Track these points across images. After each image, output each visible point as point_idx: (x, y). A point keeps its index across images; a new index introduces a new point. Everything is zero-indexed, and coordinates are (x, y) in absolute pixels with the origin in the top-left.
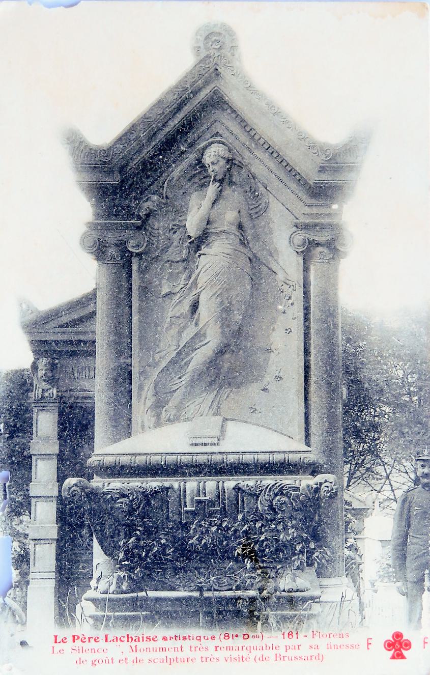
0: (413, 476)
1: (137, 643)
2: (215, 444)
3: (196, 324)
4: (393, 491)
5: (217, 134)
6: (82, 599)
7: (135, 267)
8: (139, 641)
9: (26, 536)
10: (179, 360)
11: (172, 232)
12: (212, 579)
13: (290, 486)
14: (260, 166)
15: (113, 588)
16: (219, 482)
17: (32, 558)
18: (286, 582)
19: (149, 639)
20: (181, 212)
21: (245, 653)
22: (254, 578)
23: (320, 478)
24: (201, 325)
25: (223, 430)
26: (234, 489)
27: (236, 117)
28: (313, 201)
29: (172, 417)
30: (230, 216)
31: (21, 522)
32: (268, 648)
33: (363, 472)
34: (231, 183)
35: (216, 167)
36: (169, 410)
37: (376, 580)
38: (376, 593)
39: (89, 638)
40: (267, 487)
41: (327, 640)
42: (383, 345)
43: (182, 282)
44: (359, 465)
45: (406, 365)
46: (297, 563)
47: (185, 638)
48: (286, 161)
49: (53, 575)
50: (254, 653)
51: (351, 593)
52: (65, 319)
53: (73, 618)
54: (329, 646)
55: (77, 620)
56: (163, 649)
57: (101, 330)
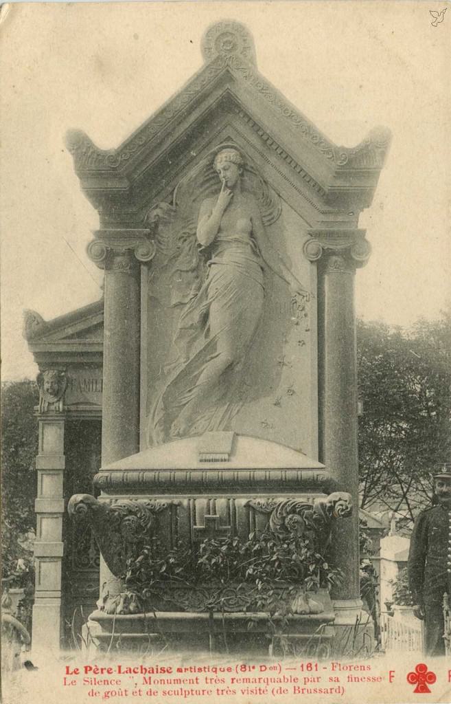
0: (430, 495)
1: (151, 675)
2: (225, 460)
3: (207, 336)
4: (410, 510)
5: (229, 139)
6: (89, 619)
7: (143, 277)
8: (153, 672)
9: (31, 553)
10: (187, 376)
11: (182, 240)
12: (223, 599)
13: (302, 504)
14: (274, 171)
15: (119, 609)
16: (229, 500)
17: (37, 575)
18: (298, 604)
19: (163, 670)
20: (189, 220)
21: (263, 686)
22: (265, 599)
23: (334, 496)
24: (212, 335)
25: (234, 442)
26: (245, 506)
27: (249, 121)
28: (326, 208)
29: (181, 432)
30: (242, 223)
31: (27, 539)
32: (286, 680)
33: (378, 490)
34: (243, 190)
35: (228, 174)
36: (180, 424)
37: (393, 603)
38: (392, 616)
39: (102, 669)
40: (279, 505)
41: (347, 673)
42: (401, 358)
43: (192, 292)
44: (375, 483)
45: (423, 378)
46: (310, 585)
47: (200, 670)
48: (295, 162)
49: (59, 594)
50: (272, 686)
51: (366, 617)
52: (70, 331)
53: (79, 640)
54: (350, 679)
55: (83, 641)
56: (178, 681)
57: (108, 341)
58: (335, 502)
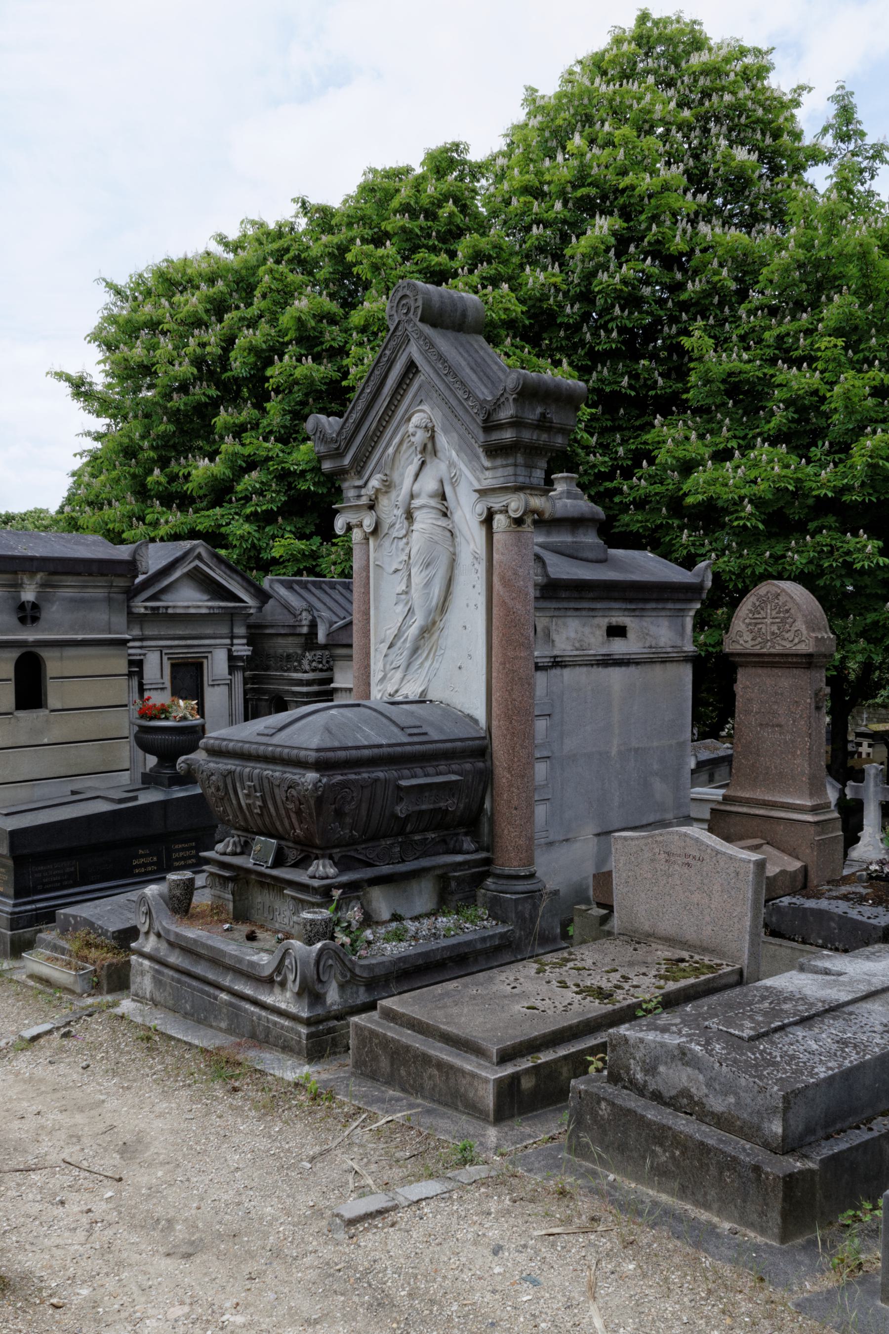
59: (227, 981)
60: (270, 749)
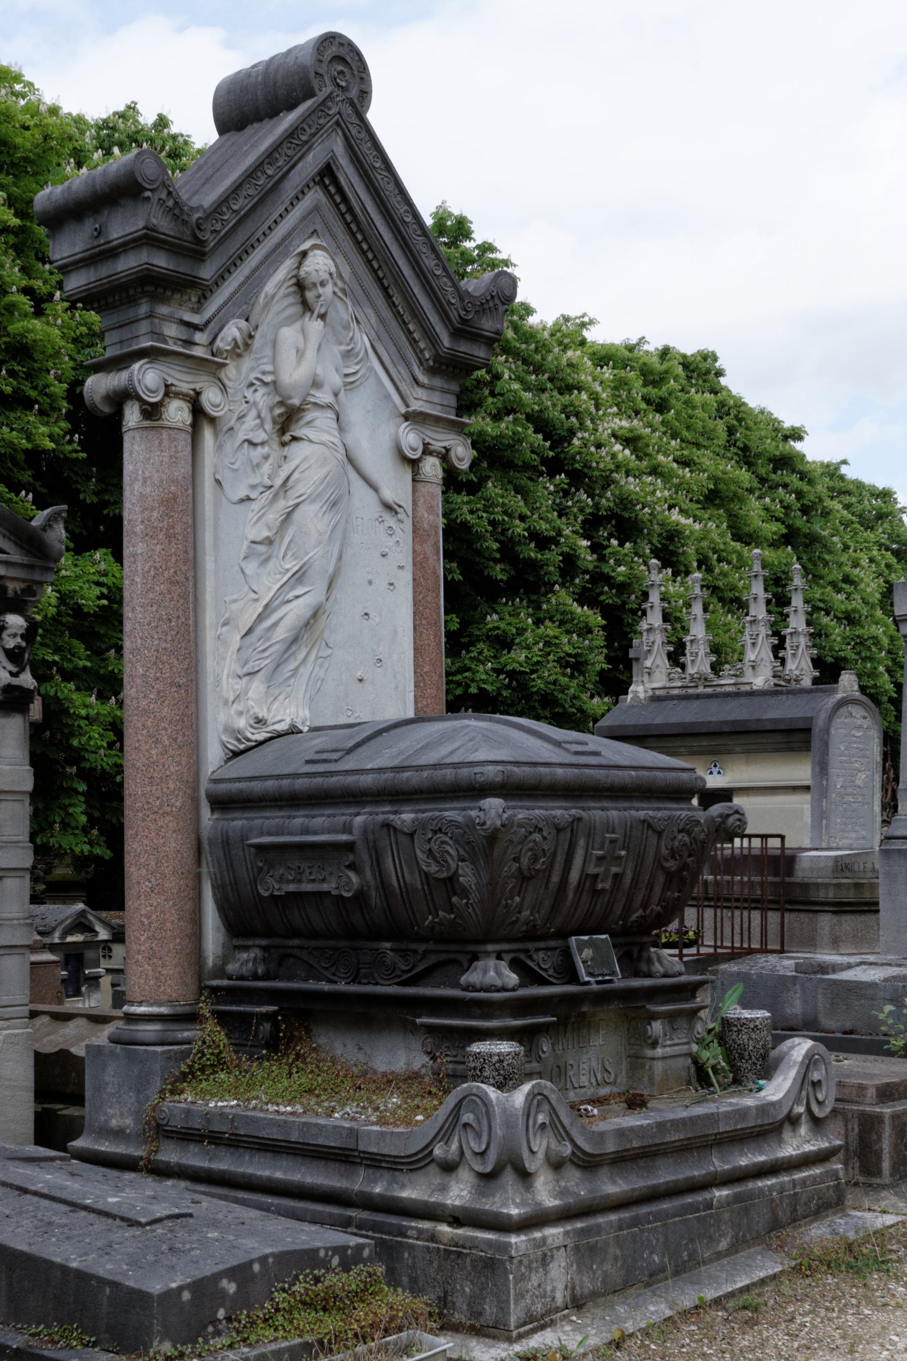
58: (728, 816)
59: (718, 1164)
60: (426, 774)
